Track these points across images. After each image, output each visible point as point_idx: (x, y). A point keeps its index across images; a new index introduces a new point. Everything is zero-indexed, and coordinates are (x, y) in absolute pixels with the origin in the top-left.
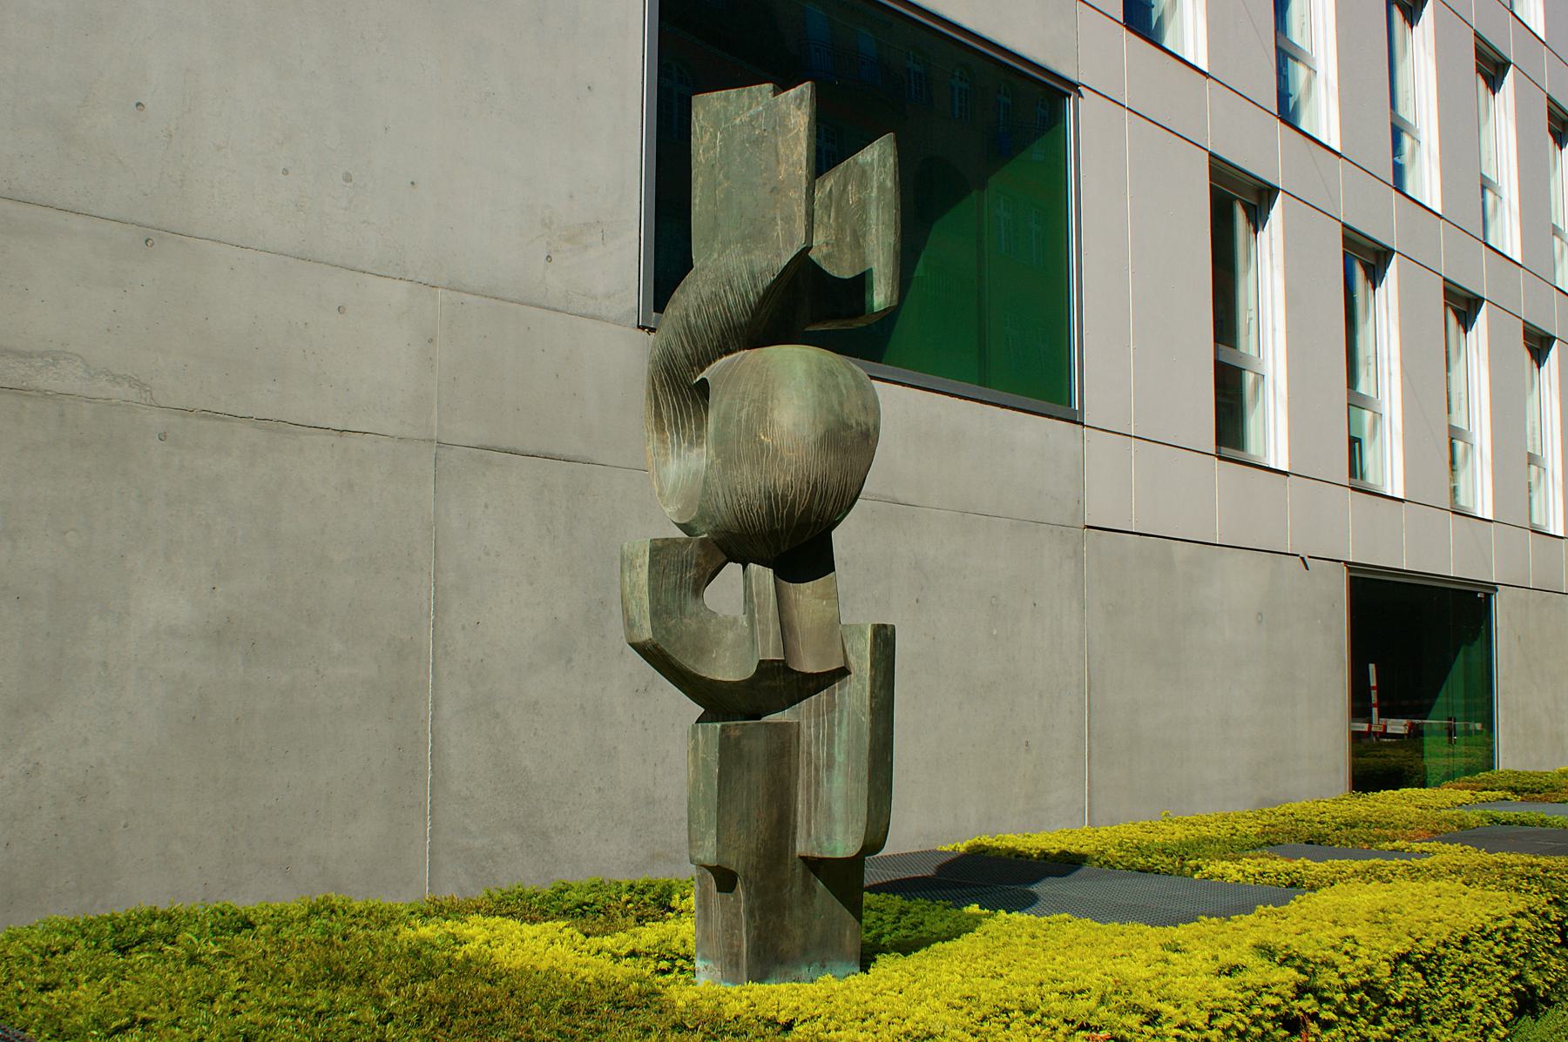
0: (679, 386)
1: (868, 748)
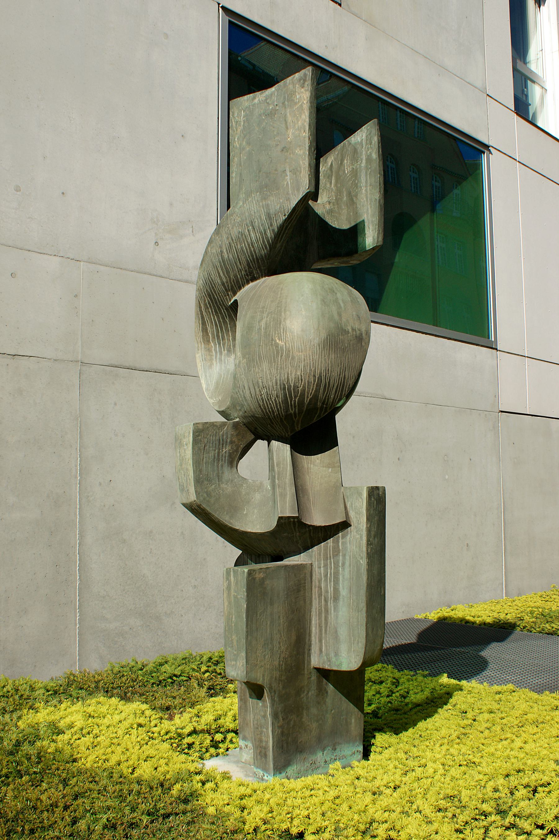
0: (218, 306)
1: (365, 585)
